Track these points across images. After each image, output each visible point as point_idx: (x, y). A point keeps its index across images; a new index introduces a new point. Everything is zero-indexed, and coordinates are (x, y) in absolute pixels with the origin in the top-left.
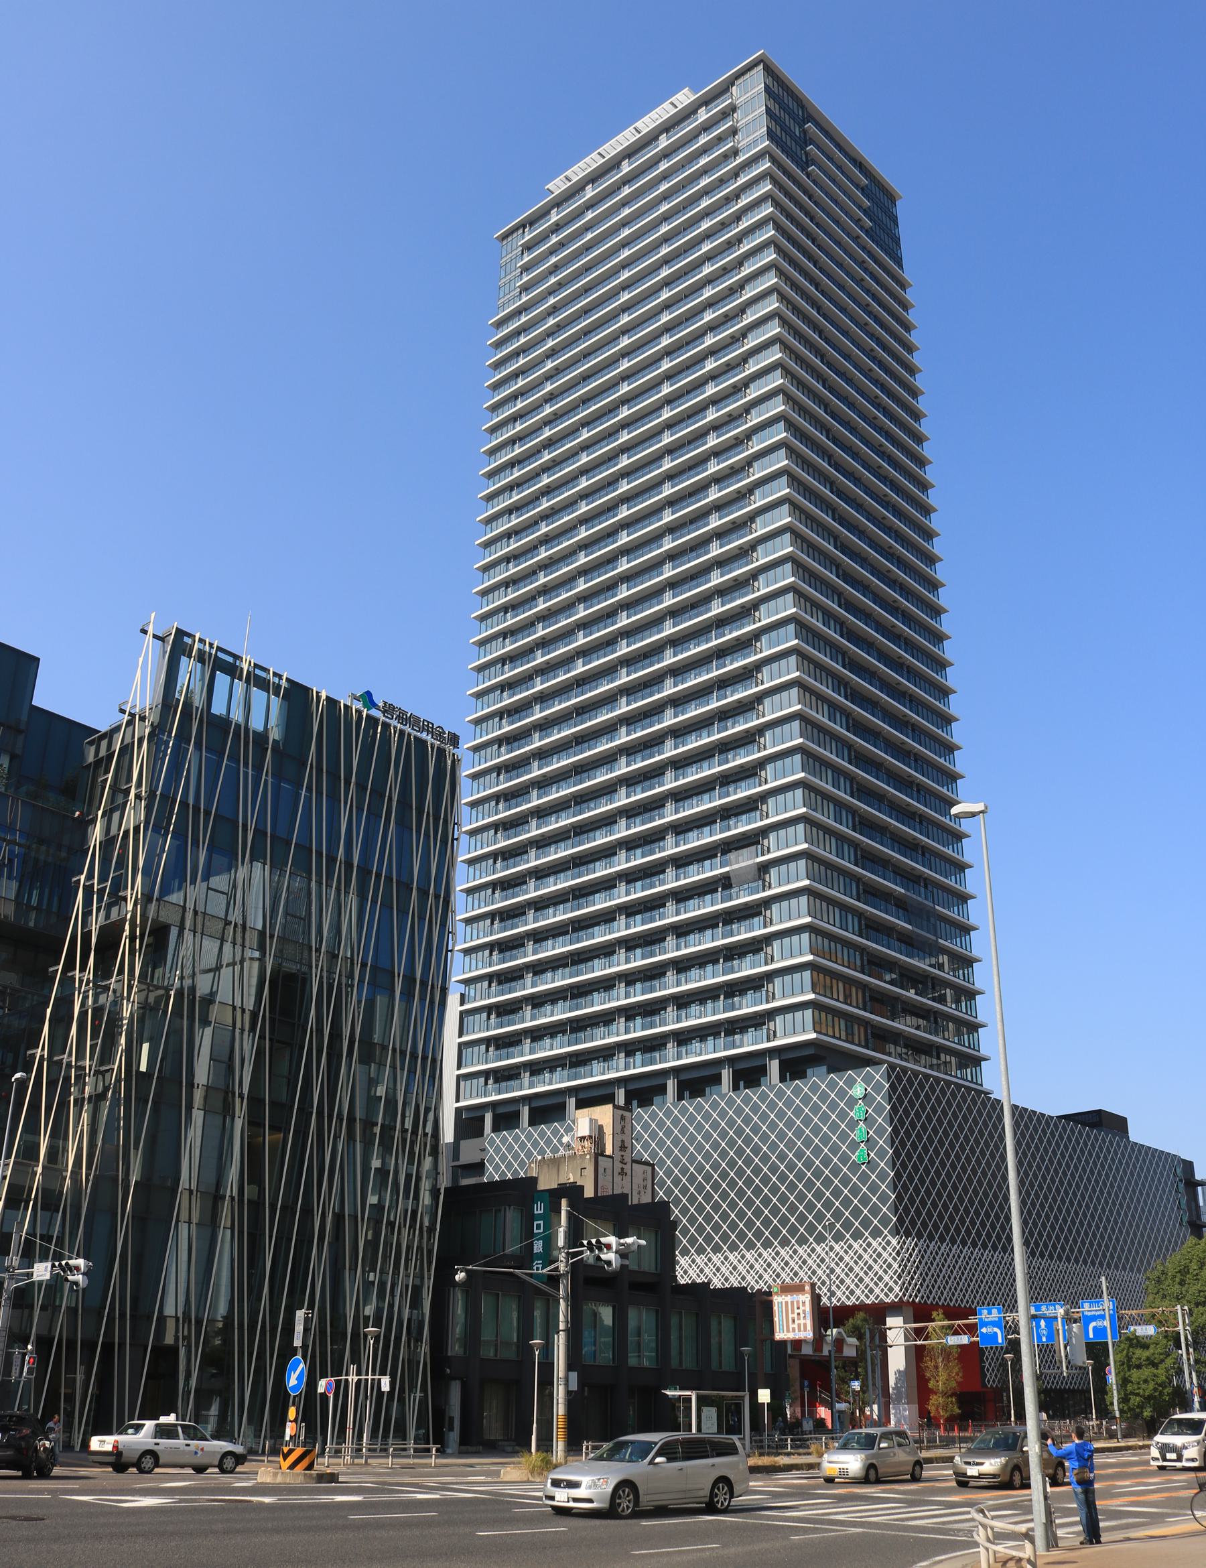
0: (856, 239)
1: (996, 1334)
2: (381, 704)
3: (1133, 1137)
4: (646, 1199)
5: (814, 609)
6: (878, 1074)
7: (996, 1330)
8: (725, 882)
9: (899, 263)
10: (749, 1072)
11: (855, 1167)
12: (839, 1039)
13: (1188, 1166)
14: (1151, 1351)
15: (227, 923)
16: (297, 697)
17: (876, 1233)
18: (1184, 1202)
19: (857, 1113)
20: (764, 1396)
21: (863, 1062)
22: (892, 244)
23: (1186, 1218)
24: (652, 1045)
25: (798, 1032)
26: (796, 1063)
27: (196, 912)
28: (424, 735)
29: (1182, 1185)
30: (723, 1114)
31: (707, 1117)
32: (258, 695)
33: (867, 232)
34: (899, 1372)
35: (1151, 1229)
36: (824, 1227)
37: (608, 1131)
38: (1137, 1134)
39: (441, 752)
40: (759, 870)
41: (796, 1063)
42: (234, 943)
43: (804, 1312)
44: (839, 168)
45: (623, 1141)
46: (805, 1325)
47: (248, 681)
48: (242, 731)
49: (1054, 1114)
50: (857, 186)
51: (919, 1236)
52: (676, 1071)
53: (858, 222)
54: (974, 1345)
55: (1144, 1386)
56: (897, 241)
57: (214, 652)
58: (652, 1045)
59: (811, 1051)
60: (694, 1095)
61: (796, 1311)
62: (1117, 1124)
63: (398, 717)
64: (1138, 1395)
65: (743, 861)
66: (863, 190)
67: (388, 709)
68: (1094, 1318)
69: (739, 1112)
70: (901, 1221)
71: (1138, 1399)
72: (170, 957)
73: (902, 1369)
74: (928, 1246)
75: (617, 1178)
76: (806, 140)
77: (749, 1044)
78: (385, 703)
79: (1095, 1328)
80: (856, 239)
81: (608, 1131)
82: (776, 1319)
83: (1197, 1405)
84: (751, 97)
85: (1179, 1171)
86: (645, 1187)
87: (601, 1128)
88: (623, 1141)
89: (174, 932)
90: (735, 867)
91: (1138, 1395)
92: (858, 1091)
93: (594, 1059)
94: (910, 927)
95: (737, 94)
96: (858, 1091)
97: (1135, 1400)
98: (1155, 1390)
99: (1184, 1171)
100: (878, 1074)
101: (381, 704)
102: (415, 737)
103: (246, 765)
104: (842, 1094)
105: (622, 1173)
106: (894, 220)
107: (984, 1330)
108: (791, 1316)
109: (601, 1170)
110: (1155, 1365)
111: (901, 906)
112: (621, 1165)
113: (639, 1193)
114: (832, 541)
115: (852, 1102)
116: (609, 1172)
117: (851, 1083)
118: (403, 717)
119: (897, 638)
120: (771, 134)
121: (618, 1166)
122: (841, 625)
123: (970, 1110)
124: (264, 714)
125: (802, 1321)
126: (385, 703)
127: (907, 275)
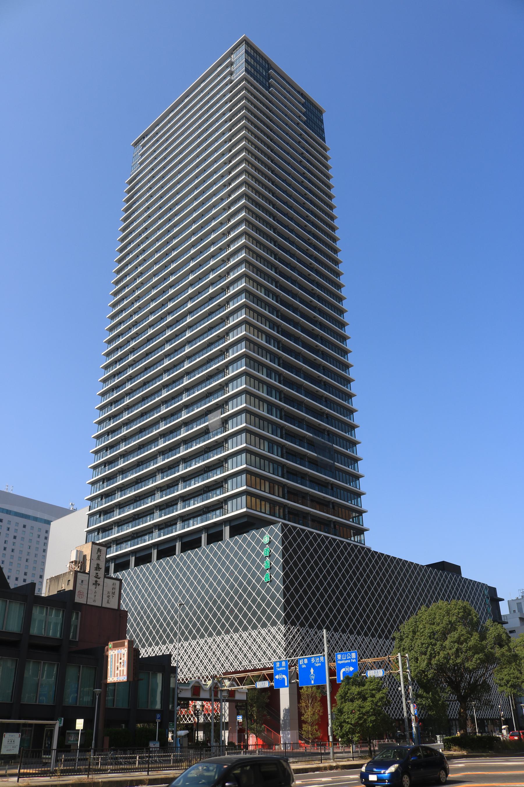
0: (298, 124)
1: (284, 679)
4: (21, 583)
6: (276, 529)
7: (284, 676)
8: (206, 432)
9: (324, 140)
10: (214, 535)
11: (263, 585)
12: (265, 513)
14: (366, 687)
17: (274, 624)
18: (490, 610)
20: (80, 724)
21: (267, 523)
22: (320, 132)
24: (169, 524)
25: (237, 509)
26: (241, 526)
29: (488, 601)
33: (304, 123)
34: (285, 709)
37: (88, 558)
38: (465, 574)
40: (223, 423)
41: (241, 526)
43: (123, 660)
44: (289, 92)
45: (98, 565)
46: (123, 670)
49: (424, 564)
50: (300, 103)
52: (180, 537)
53: (299, 117)
54: (271, 687)
55: (351, 716)
56: (323, 130)
58: (169, 524)
59: (245, 520)
61: (120, 661)
62: (456, 569)
64: (348, 723)
65: (215, 418)
66: (303, 105)
70: (288, 616)
71: (349, 726)
73: (287, 708)
75: (92, 587)
76: (269, 77)
77: (215, 518)
79: (344, 672)
80: (298, 124)
81: (88, 558)
82: (109, 667)
84: (240, 57)
86: (114, 593)
87: (85, 557)
88: (98, 565)
90: (211, 422)
91: (348, 723)
94: (316, 455)
95: (234, 57)
96: (266, 540)
97: (347, 727)
98: (360, 718)
100: (276, 529)
104: (258, 542)
105: (96, 584)
106: (322, 121)
107: (277, 677)
108: (116, 664)
109: (79, 581)
110: (365, 699)
111: (311, 444)
112: (95, 579)
113: (108, 597)
115: (263, 546)
116: (85, 583)
117: (263, 535)
119: (314, 308)
120: (247, 70)
121: (93, 579)
122: (277, 297)
123: (414, 583)
125: (122, 669)
127: (327, 145)
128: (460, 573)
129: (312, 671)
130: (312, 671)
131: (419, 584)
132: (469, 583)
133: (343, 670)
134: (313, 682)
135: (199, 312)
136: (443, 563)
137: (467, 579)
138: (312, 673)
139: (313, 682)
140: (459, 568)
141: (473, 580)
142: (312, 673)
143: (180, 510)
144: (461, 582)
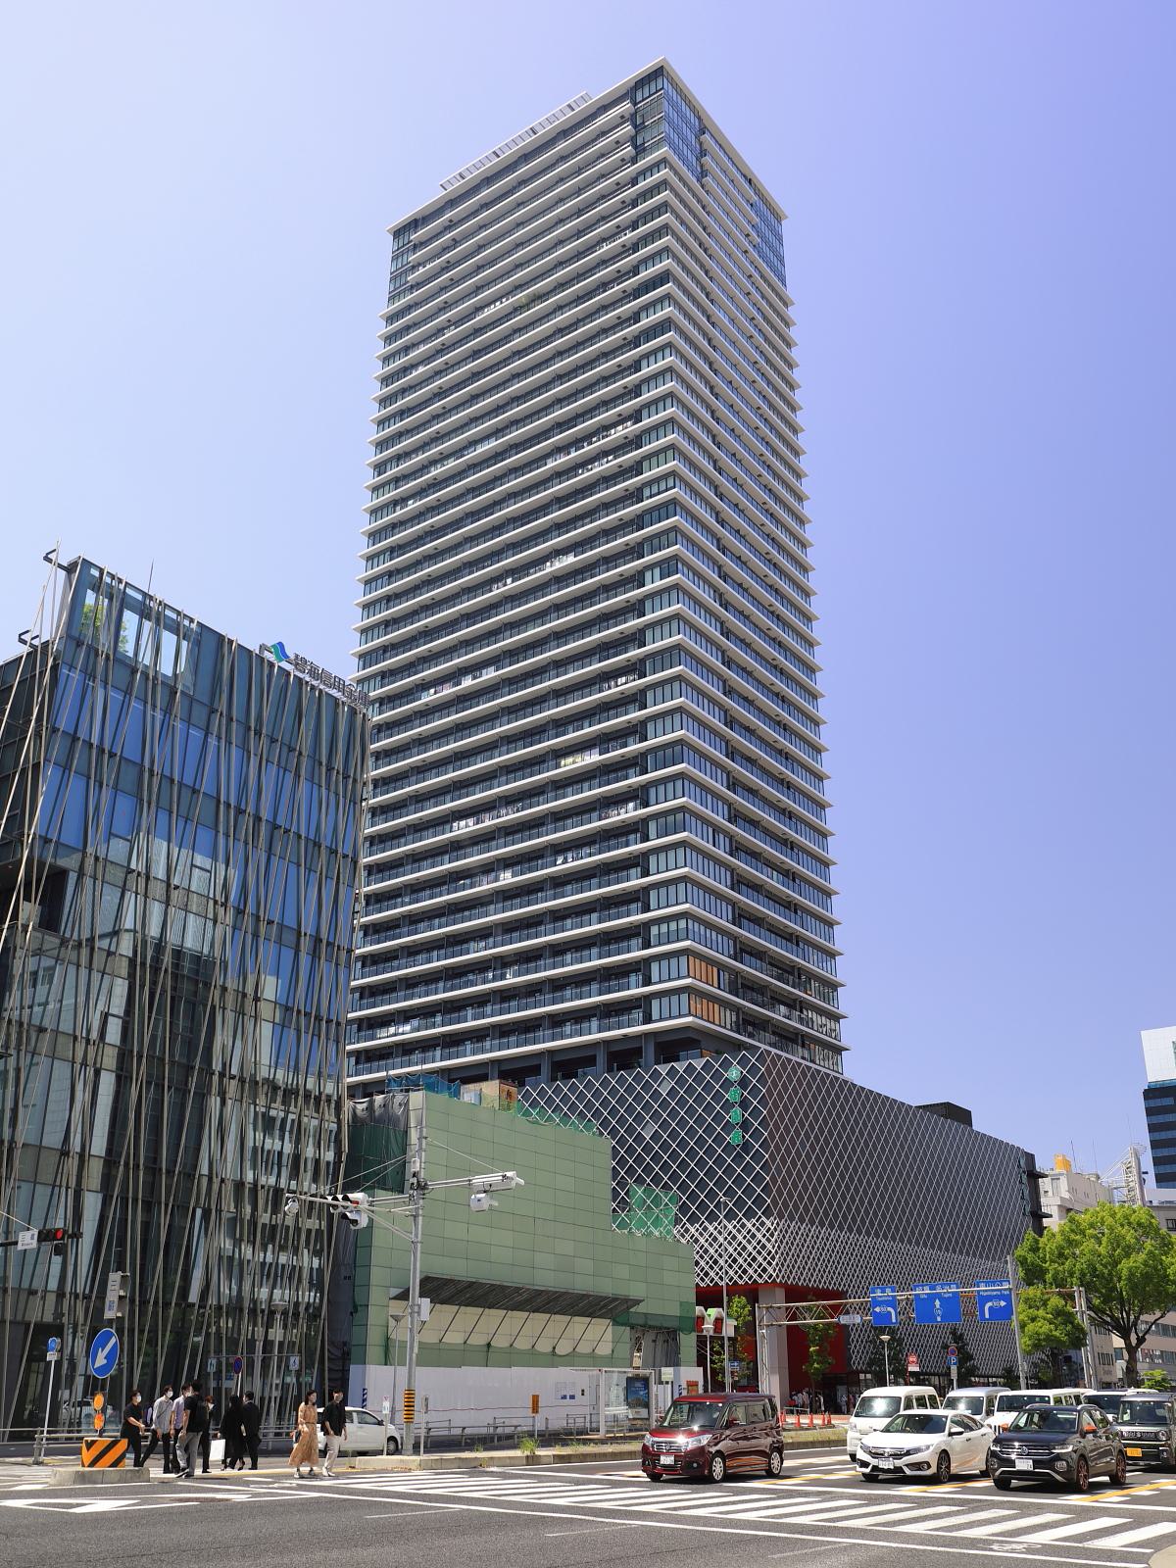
1: (890, 1313)
2: (292, 657)
3: (976, 1127)
5: (697, 607)
7: (889, 1309)
11: (728, 1149)
13: (1030, 1158)
15: (130, 871)
16: (208, 645)
18: (1026, 1192)
19: (733, 1095)
23: (1028, 1209)
27: (97, 859)
28: (334, 692)
29: (1025, 1177)
30: (597, 1094)
31: (581, 1097)
32: (169, 640)
35: (948, 1222)
36: (726, 1205)
38: (979, 1125)
39: (353, 712)
42: (219, 738)
47: (158, 623)
48: (151, 678)
49: (914, 1104)
51: (781, 1216)
56: (782, 261)
57: (122, 586)
60: (567, 1077)
62: (962, 1116)
63: (310, 671)
67: (299, 662)
68: (990, 1298)
69: (613, 1092)
72: (63, 928)
74: (789, 1226)
78: (297, 656)
79: (990, 1308)
83: (1022, 1381)
85: (1022, 1163)
89: (72, 877)
92: (734, 1074)
93: (467, 1040)
96: (734, 1074)
99: (1027, 1163)
101: (292, 657)
102: (326, 693)
103: (154, 707)
107: (877, 1309)
114: (715, 542)
115: (727, 1084)
117: (726, 1065)
118: (314, 672)
124: (169, 658)
126: (297, 656)
127: (790, 292)
128: (971, 1125)
129: (937, 1303)
130: (937, 1303)
131: (847, 1119)
132: (850, 1091)
133: (990, 1304)
134: (939, 1319)
135: (450, 486)
136: (948, 1105)
137: (863, 1089)
138: (938, 1306)
139: (939, 1319)
140: (968, 1113)
141: (867, 1087)
142: (938, 1306)
143: (477, 953)
144: (851, 1093)
